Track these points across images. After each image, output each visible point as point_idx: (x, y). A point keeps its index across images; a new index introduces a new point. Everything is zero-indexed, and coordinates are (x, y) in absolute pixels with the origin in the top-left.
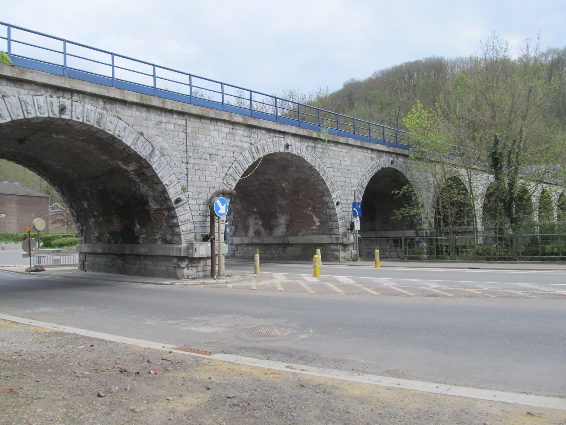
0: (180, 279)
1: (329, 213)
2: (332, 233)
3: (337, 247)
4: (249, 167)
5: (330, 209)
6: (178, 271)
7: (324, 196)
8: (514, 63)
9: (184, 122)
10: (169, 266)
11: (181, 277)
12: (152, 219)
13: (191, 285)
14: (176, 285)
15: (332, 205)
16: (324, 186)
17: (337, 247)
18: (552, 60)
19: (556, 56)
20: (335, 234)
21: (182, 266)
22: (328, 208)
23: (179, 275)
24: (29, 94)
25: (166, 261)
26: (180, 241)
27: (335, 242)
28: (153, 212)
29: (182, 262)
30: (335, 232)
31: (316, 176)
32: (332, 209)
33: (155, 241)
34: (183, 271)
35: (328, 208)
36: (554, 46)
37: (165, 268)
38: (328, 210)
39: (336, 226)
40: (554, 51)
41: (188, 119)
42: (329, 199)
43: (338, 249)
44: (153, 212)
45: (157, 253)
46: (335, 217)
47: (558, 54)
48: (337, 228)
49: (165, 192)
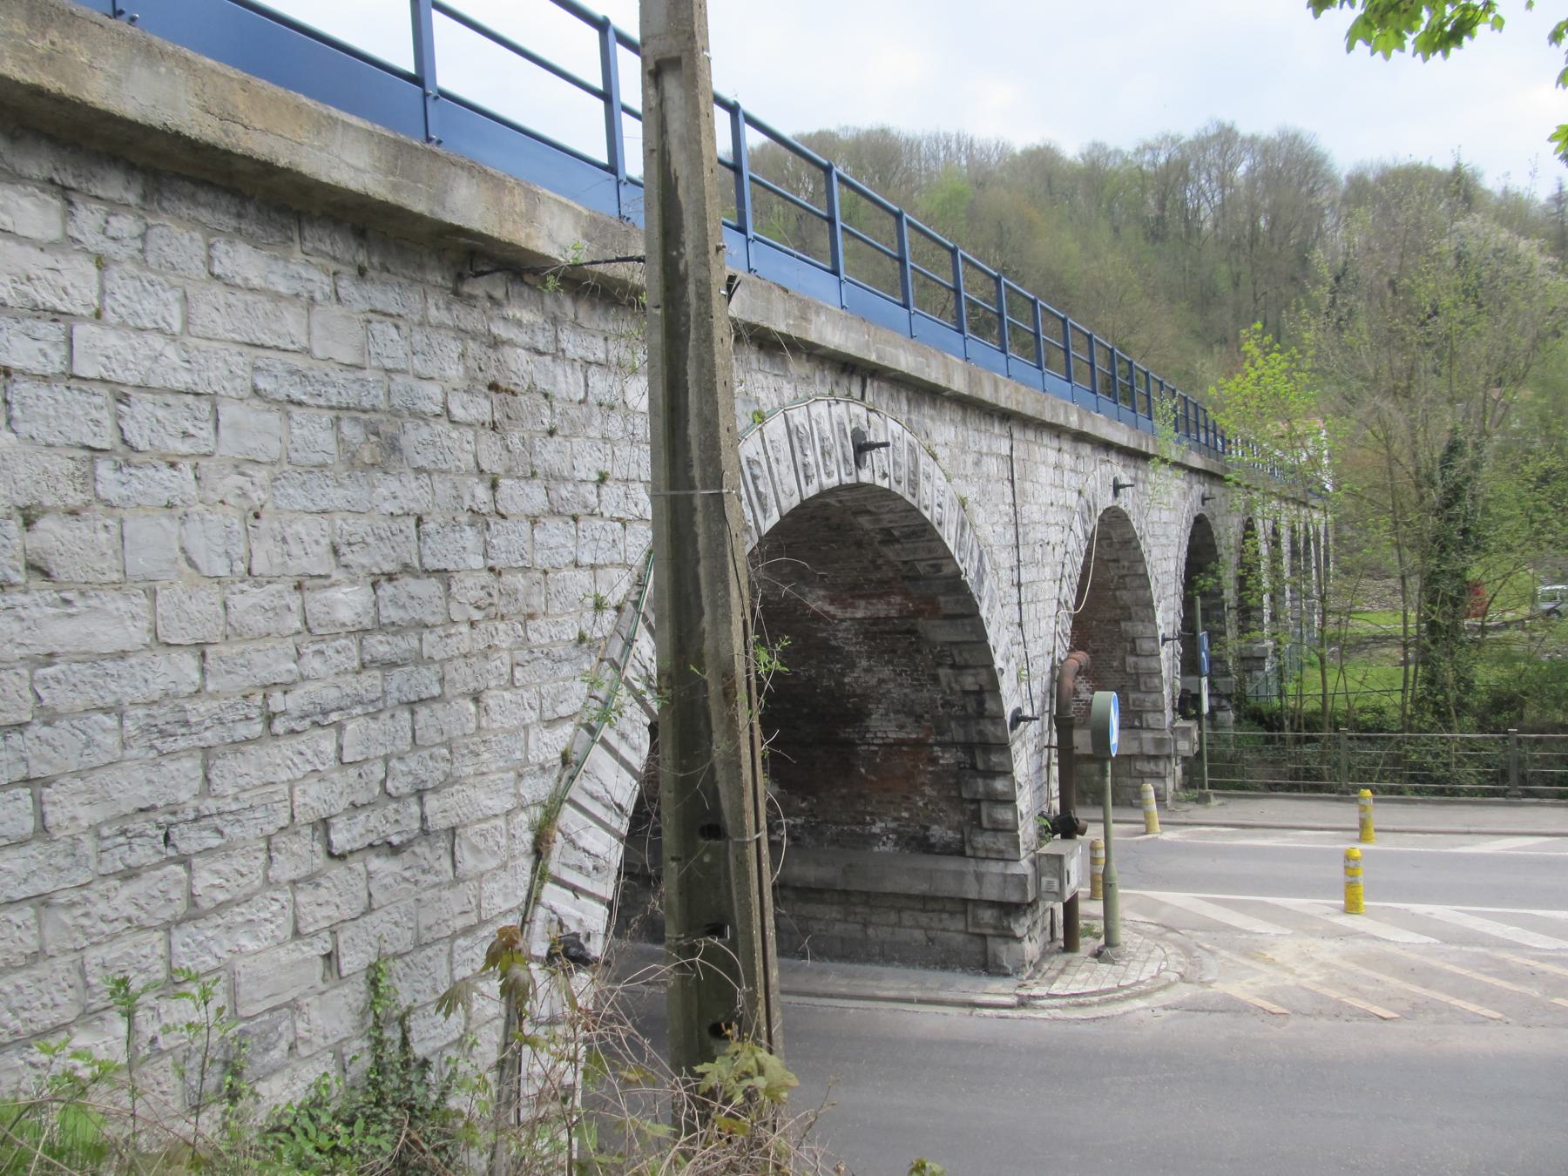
0: (1007, 975)
1: (1136, 668)
2: (1137, 723)
3: (1157, 766)
4: (804, 504)
5: (1137, 655)
6: (1004, 952)
7: (1130, 619)
8: (1071, 165)
9: (1004, 447)
10: (944, 930)
11: (1014, 970)
12: (863, 770)
13: (1099, 1004)
14: (1043, 1008)
15: (1153, 644)
16: (1141, 592)
17: (1157, 766)
18: (1168, 162)
19: (1177, 155)
20: (1149, 728)
21: (1019, 932)
22: (1134, 652)
23: (1005, 964)
24: (68, 243)
25: (923, 911)
26: (1012, 850)
27: (1153, 753)
28: (876, 748)
29: (1017, 921)
30: (1151, 722)
31: (1126, 564)
32: (1146, 656)
33: (870, 839)
34: (1023, 951)
35: (1134, 652)
36: (1173, 132)
37: (919, 935)
38: (1131, 660)
39: (1155, 703)
40: (1174, 142)
41: (1016, 435)
42: (1145, 627)
43: (1158, 773)
44: (876, 748)
45: (889, 887)
46: (1156, 681)
47: (1181, 149)
48: (1155, 711)
49: (987, 696)
